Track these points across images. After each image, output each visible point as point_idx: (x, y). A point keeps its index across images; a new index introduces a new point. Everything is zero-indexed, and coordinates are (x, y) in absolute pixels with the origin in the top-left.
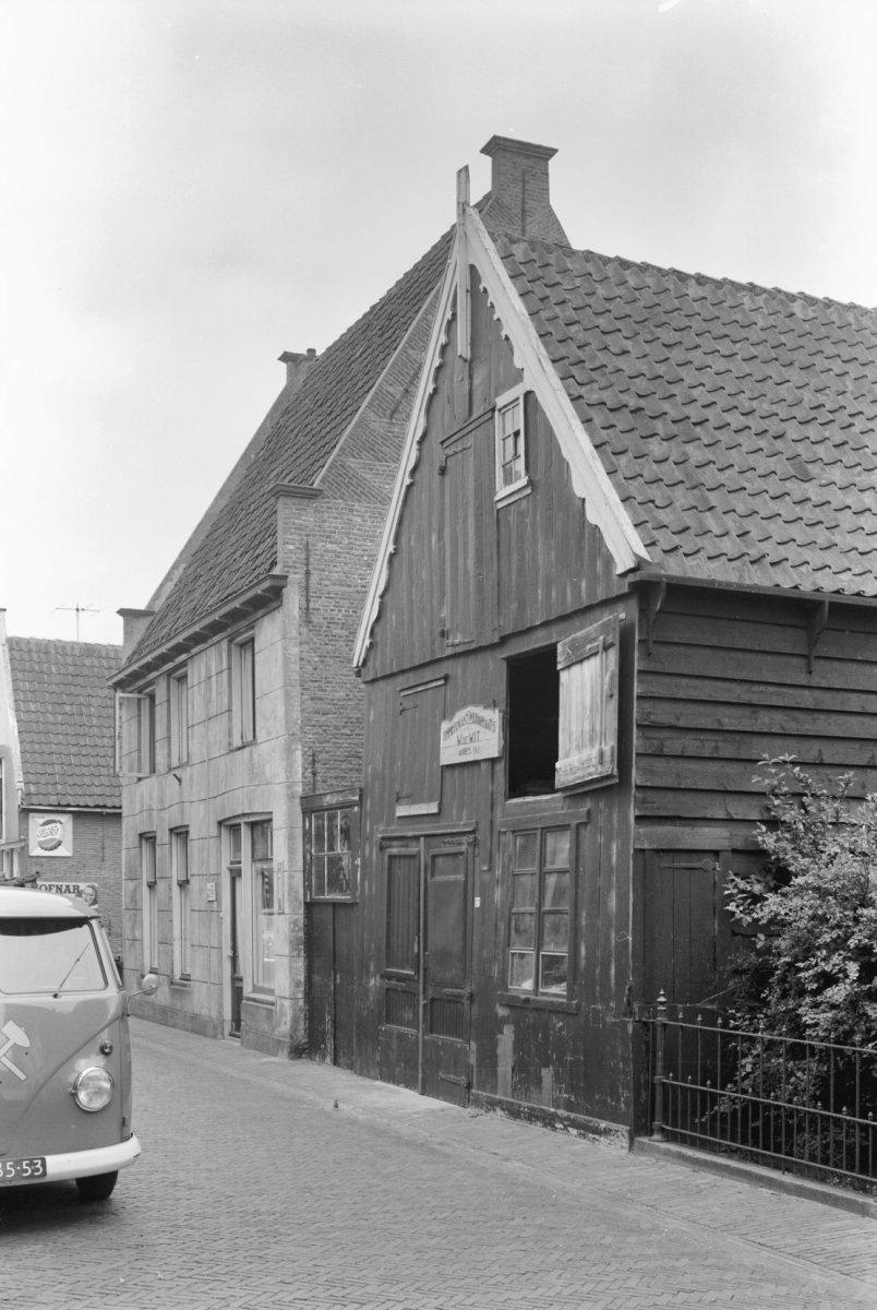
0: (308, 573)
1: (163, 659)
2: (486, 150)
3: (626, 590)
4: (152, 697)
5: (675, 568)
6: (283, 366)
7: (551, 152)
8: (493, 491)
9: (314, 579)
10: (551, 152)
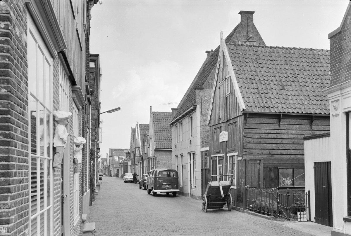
0: (201, 104)
1: (178, 120)
2: (240, 13)
3: (242, 114)
4: (177, 126)
5: (250, 110)
6: (206, 54)
7: (253, 13)
8: (226, 94)
9: (203, 105)
10: (253, 13)
